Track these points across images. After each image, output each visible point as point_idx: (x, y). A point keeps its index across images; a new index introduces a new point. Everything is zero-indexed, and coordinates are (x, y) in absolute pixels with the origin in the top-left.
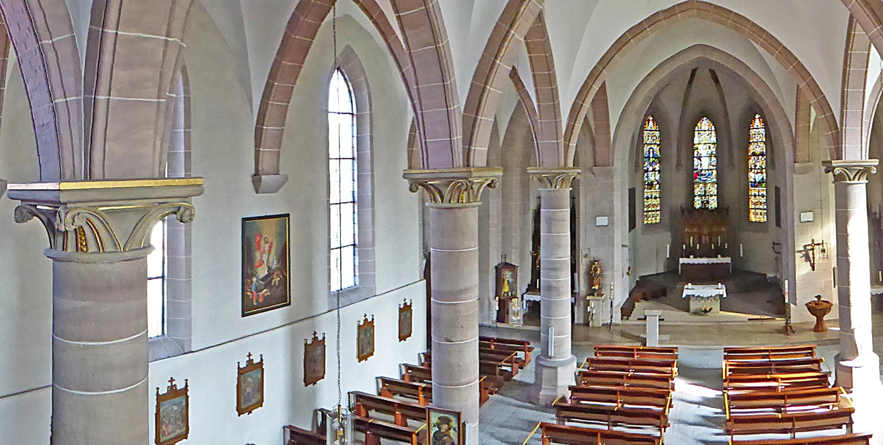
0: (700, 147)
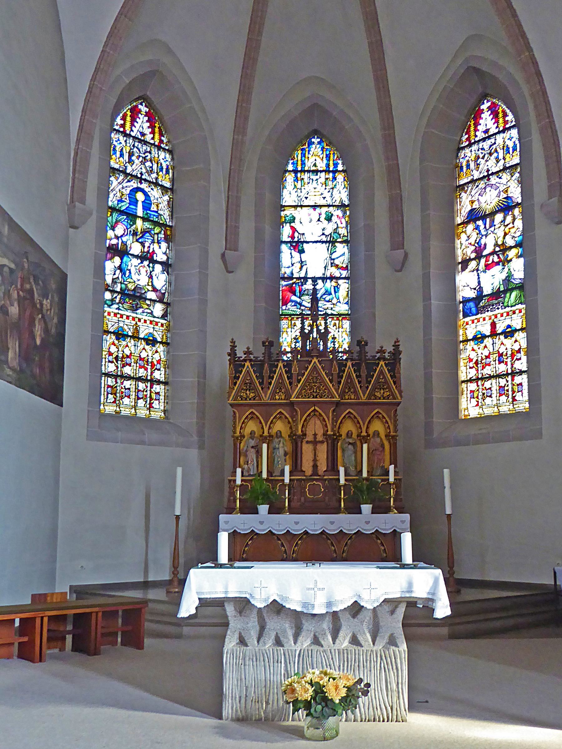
0: (299, 214)
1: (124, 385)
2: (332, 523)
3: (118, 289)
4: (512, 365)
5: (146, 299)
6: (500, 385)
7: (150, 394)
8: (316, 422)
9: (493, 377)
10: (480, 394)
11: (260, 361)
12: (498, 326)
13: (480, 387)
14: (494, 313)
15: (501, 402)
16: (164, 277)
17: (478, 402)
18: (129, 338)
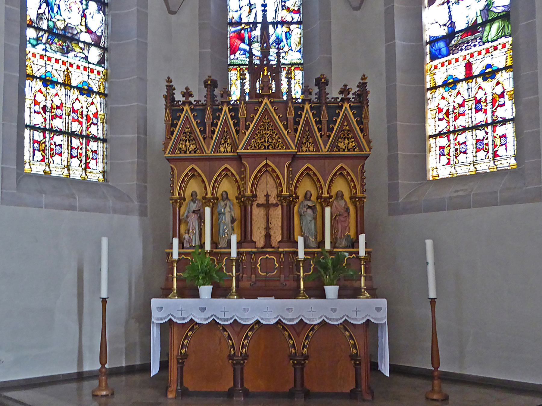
1: (54, 140)
2: (290, 310)
3: (45, 28)
4: (493, 113)
5: (78, 41)
6: (478, 138)
7: (86, 153)
8: (269, 180)
9: (469, 128)
10: (451, 150)
11: (203, 105)
12: (474, 67)
13: (453, 141)
14: (470, 51)
15: (478, 158)
16: (100, 17)
17: (449, 159)
18: (59, 85)
